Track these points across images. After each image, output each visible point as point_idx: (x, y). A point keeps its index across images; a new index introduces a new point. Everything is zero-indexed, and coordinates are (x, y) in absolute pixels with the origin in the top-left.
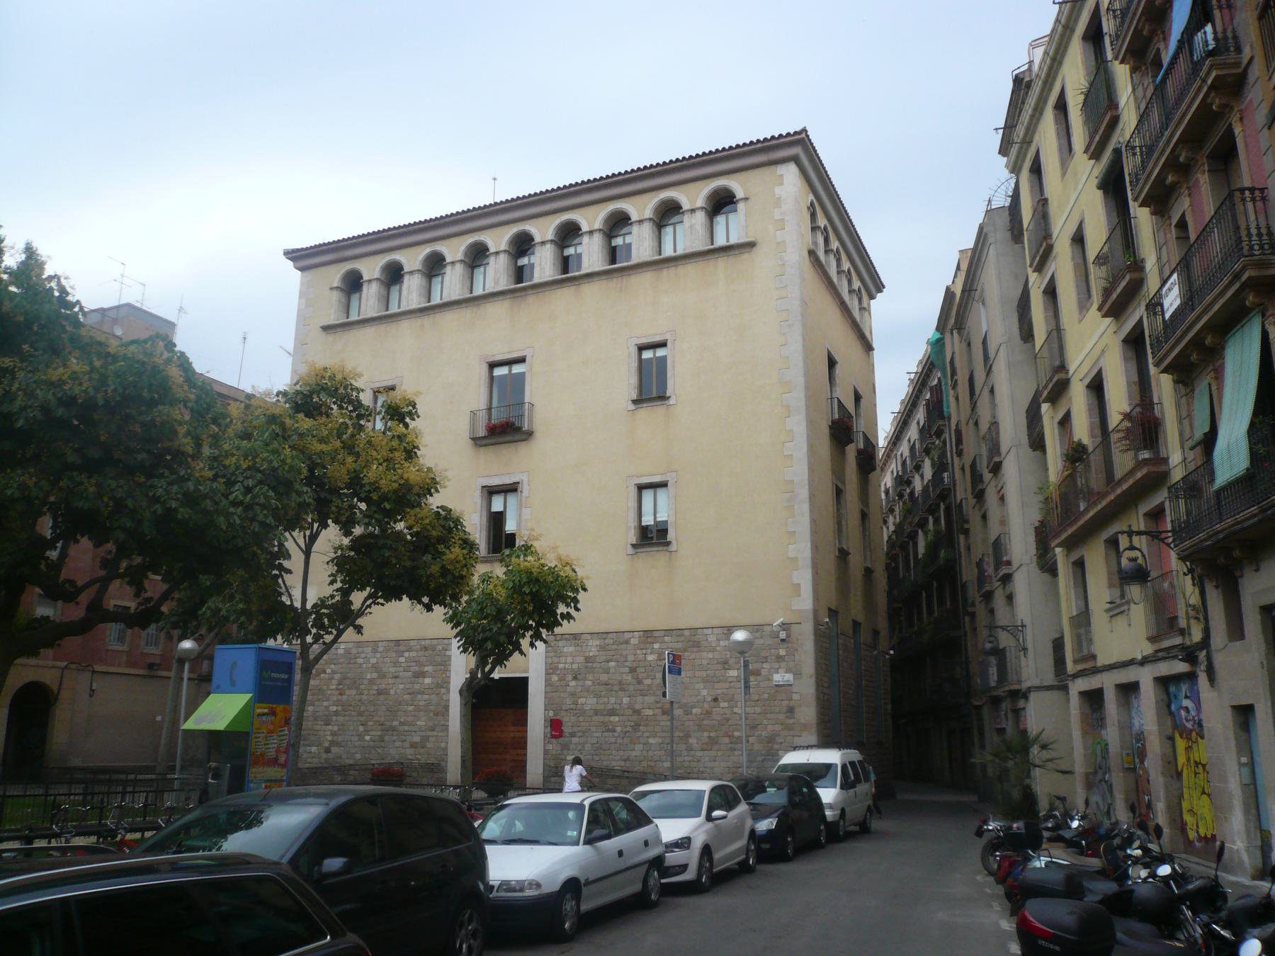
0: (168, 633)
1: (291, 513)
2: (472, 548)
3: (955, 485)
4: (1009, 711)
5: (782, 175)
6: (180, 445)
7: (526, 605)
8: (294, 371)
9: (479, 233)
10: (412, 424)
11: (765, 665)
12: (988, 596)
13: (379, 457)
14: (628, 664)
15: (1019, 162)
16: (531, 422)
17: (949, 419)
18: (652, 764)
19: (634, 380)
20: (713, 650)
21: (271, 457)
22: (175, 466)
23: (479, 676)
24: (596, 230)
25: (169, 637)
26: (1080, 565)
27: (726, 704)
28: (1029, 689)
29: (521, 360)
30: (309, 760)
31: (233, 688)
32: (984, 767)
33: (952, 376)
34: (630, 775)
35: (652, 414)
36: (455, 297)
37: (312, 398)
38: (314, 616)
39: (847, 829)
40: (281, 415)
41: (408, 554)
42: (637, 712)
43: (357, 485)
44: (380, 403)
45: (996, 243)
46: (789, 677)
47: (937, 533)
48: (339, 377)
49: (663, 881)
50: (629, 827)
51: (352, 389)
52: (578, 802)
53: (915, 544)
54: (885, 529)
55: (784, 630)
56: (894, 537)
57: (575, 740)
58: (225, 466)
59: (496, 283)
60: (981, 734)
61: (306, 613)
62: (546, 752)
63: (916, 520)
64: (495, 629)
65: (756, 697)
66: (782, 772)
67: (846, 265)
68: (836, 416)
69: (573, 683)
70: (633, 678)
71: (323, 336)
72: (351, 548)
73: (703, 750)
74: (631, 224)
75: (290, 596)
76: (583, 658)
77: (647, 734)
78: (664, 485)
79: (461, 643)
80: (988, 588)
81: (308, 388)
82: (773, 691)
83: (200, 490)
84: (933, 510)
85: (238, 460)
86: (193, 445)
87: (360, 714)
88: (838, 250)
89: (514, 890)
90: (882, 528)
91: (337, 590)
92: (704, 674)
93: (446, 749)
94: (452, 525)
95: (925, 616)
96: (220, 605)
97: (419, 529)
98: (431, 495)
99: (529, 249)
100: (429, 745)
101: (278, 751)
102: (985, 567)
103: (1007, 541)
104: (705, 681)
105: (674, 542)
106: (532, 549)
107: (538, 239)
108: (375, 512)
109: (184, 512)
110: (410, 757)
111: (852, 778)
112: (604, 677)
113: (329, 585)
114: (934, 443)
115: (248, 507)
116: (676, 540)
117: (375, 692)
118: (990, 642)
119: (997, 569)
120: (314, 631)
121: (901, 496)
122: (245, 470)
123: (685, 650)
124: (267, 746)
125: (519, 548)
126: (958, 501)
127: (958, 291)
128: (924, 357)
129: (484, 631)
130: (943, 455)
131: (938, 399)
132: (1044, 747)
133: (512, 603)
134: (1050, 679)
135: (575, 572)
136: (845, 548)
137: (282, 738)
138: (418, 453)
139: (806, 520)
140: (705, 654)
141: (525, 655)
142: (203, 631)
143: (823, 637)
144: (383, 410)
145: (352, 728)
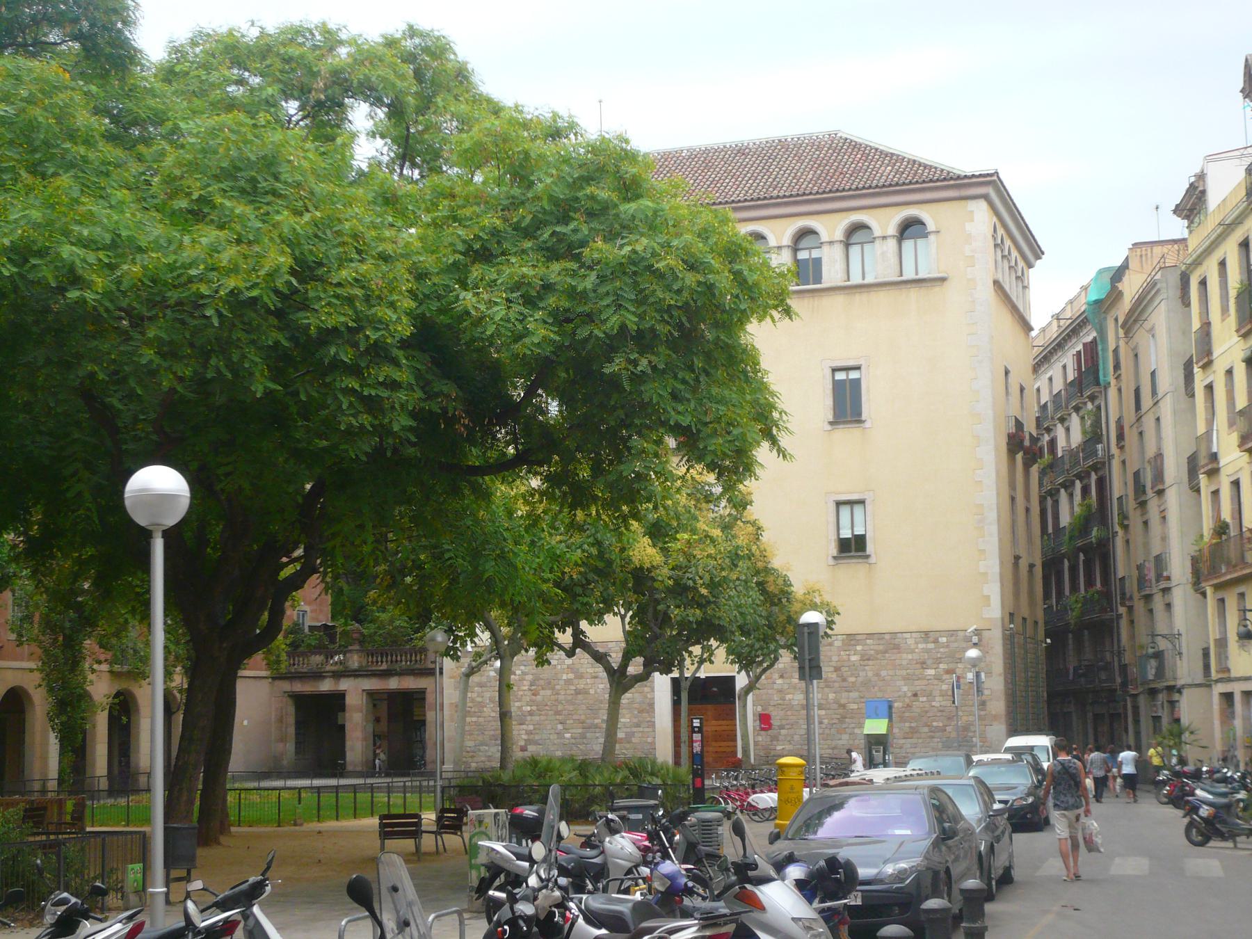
4: (1165, 703)
5: (972, 212)
11: (960, 665)
14: (834, 664)
20: (913, 652)
26: (1222, 601)
27: (925, 699)
28: (1183, 686)
35: (847, 435)
42: (843, 706)
57: (783, 732)
69: (780, 681)
70: (838, 676)
87: (558, 713)
92: (904, 673)
93: (653, 743)
100: (634, 740)
117: (573, 692)
132: (1192, 733)
134: (1199, 679)
140: (904, 656)
143: (1009, 639)
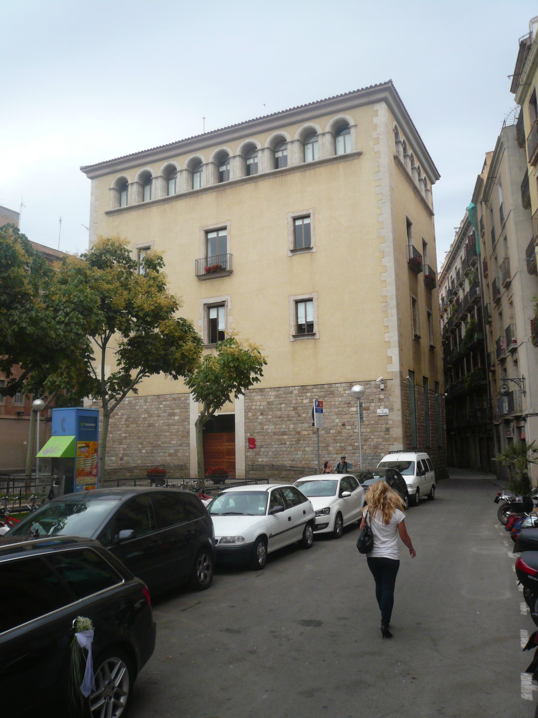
0: (27, 396)
1: (93, 327)
2: (199, 342)
3: (483, 295)
4: (515, 428)
6: (25, 290)
7: (232, 374)
8: (91, 242)
9: (196, 152)
10: (161, 270)
11: (372, 404)
12: (503, 361)
13: (142, 291)
15: (523, 97)
16: (231, 265)
17: (480, 255)
18: (307, 462)
19: (291, 238)
20: (342, 396)
21: (79, 294)
22: (24, 302)
23: (206, 414)
24: (266, 148)
25: (28, 398)
27: (350, 427)
28: (527, 416)
29: (224, 228)
30: (111, 465)
31: (64, 432)
32: (500, 462)
33: (481, 231)
34: (295, 469)
35: (302, 258)
36: (183, 191)
37: (102, 257)
38: (109, 384)
39: (420, 498)
40: (83, 268)
41: (162, 347)
42: (299, 433)
43: (130, 307)
44: (141, 259)
45: (508, 148)
46: (386, 411)
47: (473, 323)
48: (117, 244)
49: (314, 532)
50: (296, 503)
51: (125, 251)
52: (265, 490)
53: (460, 330)
54: (442, 321)
55: (382, 384)
56: (447, 326)
57: (263, 450)
58: (52, 301)
59: (207, 182)
60: (499, 441)
61: (104, 382)
62: (246, 457)
63: (460, 316)
64: (214, 388)
65: (367, 423)
66: (383, 467)
67: (417, 164)
68: (412, 256)
69: (261, 417)
70: (295, 413)
71: (106, 217)
72: (129, 344)
73: (337, 454)
74: (287, 143)
75: (95, 373)
76: (266, 402)
77: (304, 445)
78: (310, 300)
79: (195, 396)
80: (503, 356)
81: (99, 252)
82: (377, 419)
83: (39, 316)
84: (470, 310)
85: (60, 297)
86: (33, 289)
87: (139, 438)
88: (412, 155)
89: (229, 542)
90: (440, 322)
91: (122, 369)
92: (337, 410)
93: (189, 456)
94: (187, 329)
95: (466, 373)
96: (55, 379)
97: (167, 333)
98: (174, 312)
99: (226, 161)
101: (91, 468)
102: (501, 344)
103: (514, 329)
104: (337, 414)
105: (317, 334)
106: (234, 341)
107: (231, 155)
108: (141, 323)
109: (30, 329)
110: (168, 462)
111: (423, 469)
112: (278, 413)
113: (117, 366)
114: (471, 270)
115: (68, 324)
116: (319, 332)
118: (504, 388)
119: (508, 345)
120: (110, 392)
121: (451, 301)
122: (64, 303)
123: (325, 397)
124: (85, 465)
125: (227, 340)
126: (485, 305)
127: (485, 177)
128: (464, 218)
129: (208, 389)
130: (476, 277)
131: (473, 243)
132: (535, 451)
133: (224, 373)
135: (260, 353)
136: (418, 334)
137: (94, 460)
138: (165, 287)
139: (395, 319)
141: (232, 402)
142: (47, 394)
143: (405, 387)
144: (144, 263)
145: (135, 446)
